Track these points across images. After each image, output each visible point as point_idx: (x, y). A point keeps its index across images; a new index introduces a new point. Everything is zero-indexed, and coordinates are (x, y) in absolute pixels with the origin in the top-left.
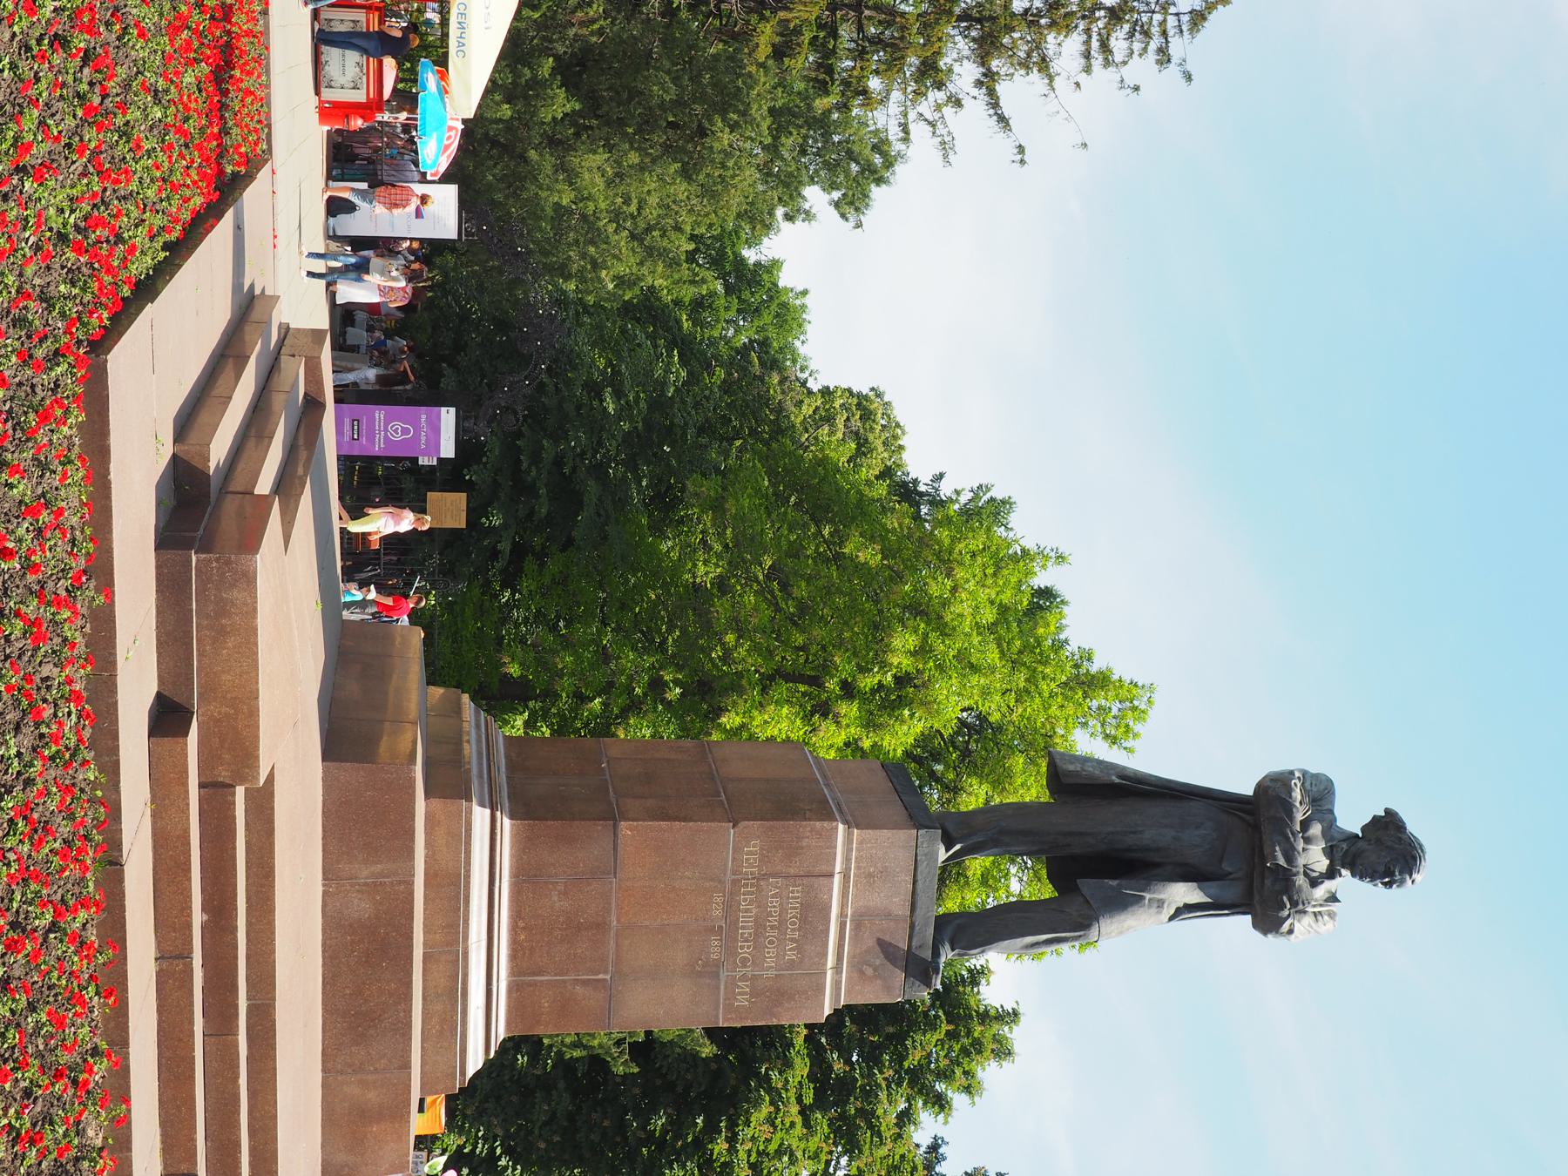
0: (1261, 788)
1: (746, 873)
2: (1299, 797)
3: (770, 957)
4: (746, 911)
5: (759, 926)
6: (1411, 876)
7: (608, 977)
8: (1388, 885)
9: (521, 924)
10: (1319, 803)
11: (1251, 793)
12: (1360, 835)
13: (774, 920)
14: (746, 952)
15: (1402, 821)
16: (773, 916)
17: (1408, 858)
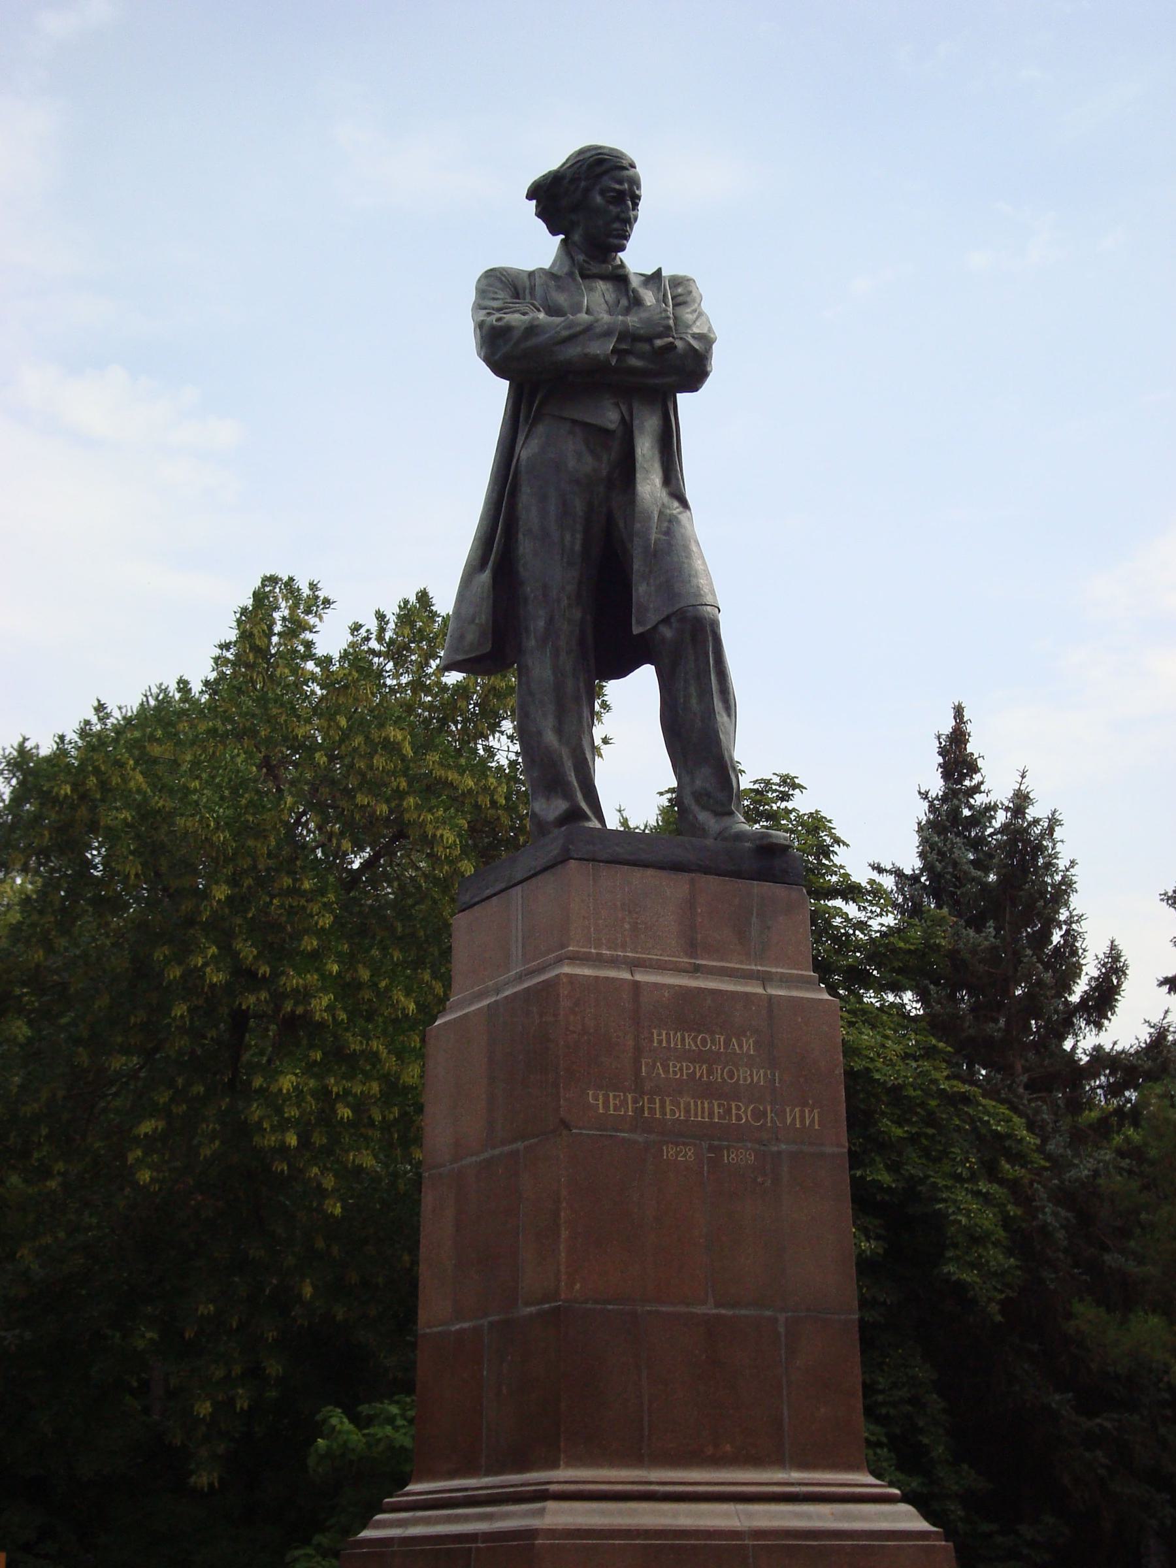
0: (498, 367)
1: (635, 1110)
2: (517, 316)
3: (751, 1075)
4: (687, 1111)
5: (708, 1091)
6: (625, 168)
7: (782, 1317)
8: (636, 199)
9: (710, 1450)
10: (521, 292)
11: (508, 382)
12: (562, 236)
13: (701, 1070)
14: (746, 1112)
15: (545, 177)
16: (694, 1072)
17: (599, 170)
